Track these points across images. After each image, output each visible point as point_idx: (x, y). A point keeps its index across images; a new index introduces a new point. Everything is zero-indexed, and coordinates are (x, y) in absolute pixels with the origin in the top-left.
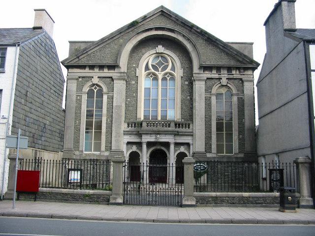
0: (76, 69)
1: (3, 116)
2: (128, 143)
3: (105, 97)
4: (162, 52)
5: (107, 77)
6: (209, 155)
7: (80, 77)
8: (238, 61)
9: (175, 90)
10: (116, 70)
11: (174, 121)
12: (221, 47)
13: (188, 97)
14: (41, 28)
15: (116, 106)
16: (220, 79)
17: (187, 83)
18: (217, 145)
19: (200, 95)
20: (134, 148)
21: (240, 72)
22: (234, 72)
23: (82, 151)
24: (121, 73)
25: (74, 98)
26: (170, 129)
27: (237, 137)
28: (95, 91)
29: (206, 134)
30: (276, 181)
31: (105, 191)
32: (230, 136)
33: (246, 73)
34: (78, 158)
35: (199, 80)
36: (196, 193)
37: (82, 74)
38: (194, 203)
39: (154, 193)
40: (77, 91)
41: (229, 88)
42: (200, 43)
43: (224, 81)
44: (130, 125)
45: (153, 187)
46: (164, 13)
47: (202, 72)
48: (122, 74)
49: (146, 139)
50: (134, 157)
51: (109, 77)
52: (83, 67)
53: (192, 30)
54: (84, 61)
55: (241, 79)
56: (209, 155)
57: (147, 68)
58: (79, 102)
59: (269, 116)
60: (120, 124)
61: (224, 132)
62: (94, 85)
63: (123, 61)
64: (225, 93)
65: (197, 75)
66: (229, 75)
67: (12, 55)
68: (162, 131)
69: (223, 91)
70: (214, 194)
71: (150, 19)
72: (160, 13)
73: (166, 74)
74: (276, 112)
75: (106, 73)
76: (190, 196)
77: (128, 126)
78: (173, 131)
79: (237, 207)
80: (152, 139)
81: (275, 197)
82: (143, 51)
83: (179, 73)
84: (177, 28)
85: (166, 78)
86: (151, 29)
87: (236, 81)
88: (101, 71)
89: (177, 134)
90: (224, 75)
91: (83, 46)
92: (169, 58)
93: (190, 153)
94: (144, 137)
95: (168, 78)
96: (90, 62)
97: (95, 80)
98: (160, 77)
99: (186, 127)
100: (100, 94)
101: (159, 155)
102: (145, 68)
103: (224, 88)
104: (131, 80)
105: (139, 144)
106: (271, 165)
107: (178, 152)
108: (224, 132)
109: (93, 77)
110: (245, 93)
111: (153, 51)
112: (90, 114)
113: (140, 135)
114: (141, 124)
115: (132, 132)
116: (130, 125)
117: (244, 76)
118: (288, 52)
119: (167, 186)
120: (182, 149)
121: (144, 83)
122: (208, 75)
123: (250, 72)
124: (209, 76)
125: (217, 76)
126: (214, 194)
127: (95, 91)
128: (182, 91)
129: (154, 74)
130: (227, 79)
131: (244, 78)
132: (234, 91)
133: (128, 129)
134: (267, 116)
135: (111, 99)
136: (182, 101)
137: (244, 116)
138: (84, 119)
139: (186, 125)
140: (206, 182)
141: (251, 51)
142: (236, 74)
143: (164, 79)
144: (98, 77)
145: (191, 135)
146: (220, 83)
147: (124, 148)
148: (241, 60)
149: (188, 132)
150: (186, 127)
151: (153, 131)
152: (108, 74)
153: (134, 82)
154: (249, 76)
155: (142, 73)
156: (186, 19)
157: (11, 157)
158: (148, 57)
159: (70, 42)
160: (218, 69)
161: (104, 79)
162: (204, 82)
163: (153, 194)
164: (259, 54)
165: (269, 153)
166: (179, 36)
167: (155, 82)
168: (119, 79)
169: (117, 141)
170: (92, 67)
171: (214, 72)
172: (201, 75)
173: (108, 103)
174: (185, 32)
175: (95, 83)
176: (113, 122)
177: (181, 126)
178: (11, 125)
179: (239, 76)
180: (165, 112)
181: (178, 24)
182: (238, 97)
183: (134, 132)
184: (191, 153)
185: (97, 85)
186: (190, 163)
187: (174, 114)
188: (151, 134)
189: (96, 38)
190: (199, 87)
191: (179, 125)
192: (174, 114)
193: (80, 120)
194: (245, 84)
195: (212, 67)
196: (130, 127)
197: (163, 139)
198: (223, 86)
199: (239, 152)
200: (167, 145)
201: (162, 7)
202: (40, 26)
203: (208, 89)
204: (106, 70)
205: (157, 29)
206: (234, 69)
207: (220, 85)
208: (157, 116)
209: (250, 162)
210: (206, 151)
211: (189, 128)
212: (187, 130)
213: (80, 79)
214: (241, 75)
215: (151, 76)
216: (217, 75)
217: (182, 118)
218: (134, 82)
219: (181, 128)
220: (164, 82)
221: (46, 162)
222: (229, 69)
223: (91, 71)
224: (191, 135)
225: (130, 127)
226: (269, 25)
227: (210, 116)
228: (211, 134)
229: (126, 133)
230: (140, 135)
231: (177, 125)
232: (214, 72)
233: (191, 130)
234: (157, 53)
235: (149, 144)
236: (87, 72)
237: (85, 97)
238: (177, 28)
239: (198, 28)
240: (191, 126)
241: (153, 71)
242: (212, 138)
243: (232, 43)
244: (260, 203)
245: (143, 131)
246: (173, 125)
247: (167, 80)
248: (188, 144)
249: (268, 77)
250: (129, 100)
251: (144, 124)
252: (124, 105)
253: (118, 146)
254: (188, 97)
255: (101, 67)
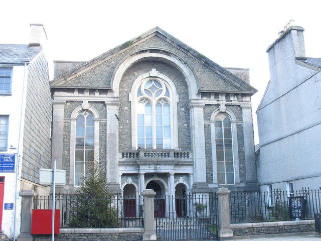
0: (66, 93)
1: (11, 146)
2: (124, 175)
3: (97, 124)
4: (156, 76)
5: (98, 102)
6: (211, 186)
7: (67, 102)
8: (236, 87)
9: (171, 116)
10: (109, 94)
11: (173, 150)
12: (219, 73)
13: (186, 125)
14: (38, 45)
15: (110, 134)
16: (219, 105)
17: (183, 109)
18: (218, 175)
19: (199, 123)
20: (130, 181)
21: (238, 99)
22: (232, 98)
23: (73, 185)
24: (114, 97)
25: (62, 125)
26: (170, 159)
27: (237, 166)
28: (85, 117)
29: (206, 164)
30: (298, 209)
31: (136, 229)
32: (230, 164)
33: (244, 99)
34: (68, 193)
35: (198, 106)
36: (232, 225)
37: (76, 98)
38: (231, 235)
39: (189, 227)
40: (65, 117)
41: (91, 113)
42: (197, 66)
43: (223, 108)
44: (125, 155)
45: (187, 221)
46: (158, 35)
47: (200, 98)
48: (116, 99)
49: (144, 170)
50: (130, 189)
51: (101, 102)
52: (71, 90)
53: (189, 54)
54: (71, 82)
55: (239, 106)
56: (211, 186)
57: (139, 92)
58: (67, 129)
59: (276, 143)
60: (114, 155)
61: (225, 161)
62: (83, 110)
63: (115, 85)
64: (224, 120)
65: (195, 101)
66: (227, 101)
67: (19, 75)
68: (161, 161)
69: (222, 118)
70: (250, 225)
71: (144, 40)
72: (154, 34)
73: (160, 99)
74: (285, 140)
75: (98, 97)
76: (226, 228)
77: (123, 157)
78: (173, 161)
79: (274, 237)
80: (151, 170)
81: (310, 225)
82: (136, 74)
83: (174, 98)
84: (173, 51)
85: (159, 103)
86: (146, 51)
87: (234, 107)
88: (92, 95)
89: (177, 164)
90: (223, 100)
91: (70, 67)
92: (162, 83)
93: (189, 184)
94: (142, 167)
95: (163, 104)
96: (79, 85)
97: (86, 105)
98: (154, 102)
99: (184, 157)
100: (92, 121)
101: (156, 184)
102: (138, 94)
103: (222, 114)
104: (124, 105)
105: (135, 176)
106: (301, 192)
107: (177, 183)
108: (225, 161)
109: (82, 102)
110: (243, 119)
111: (147, 75)
112: (80, 144)
113: (137, 165)
114: (138, 154)
115: (128, 162)
116: (125, 155)
117: (241, 103)
118: (303, 80)
119: (168, 220)
120: (181, 180)
121: (138, 108)
122: (205, 101)
123: (247, 99)
124: (208, 102)
125: (215, 102)
126: (250, 225)
127: (85, 117)
128: (179, 118)
129: (147, 99)
130: (226, 105)
131: (242, 104)
132: (96, 115)
133: (123, 160)
134: (274, 144)
135: (104, 126)
136: (180, 130)
137: (243, 144)
138: (73, 150)
139: (184, 155)
140: (208, 215)
141: (247, 77)
142: (234, 100)
143: (158, 104)
144: (89, 102)
145: (191, 164)
146: (219, 110)
147: (119, 180)
148: (238, 85)
149: (188, 162)
150: (184, 157)
151: (152, 161)
152: (99, 98)
153: (126, 108)
154: (248, 103)
155: (134, 97)
156: (185, 43)
157: (24, 193)
158: (141, 80)
159: (55, 62)
160: (217, 94)
161: (95, 104)
162: (63, 106)
163: (187, 229)
164: (259, 79)
165: (277, 180)
166: (175, 59)
167: (149, 108)
168: (112, 104)
169: (113, 173)
170: (81, 91)
171: (212, 98)
172: (200, 101)
173: (101, 131)
174: (181, 55)
175: (85, 108)
176: (107, 151)
177: (179, 155)
178: (22, 156)
179: (236, 103)
180: (160, 139)
181: (174, 47)
182: (237, 125)
183: (130, 162)
184: (192, 184)
185: (87, 110)
186: (224, 194)
187: (171, 142)
188: (150, 164)
189: (87, 59)
190: (197, 114)
191: (178, 154)
192: (171, 142)
193: (69, 150)
194: (244, 110)
195: (210, 93)
196: (132, 158)
197: (163, 169)
198: (221, 112)
199: (240, 182)
200: (166, 176)
201: (157, 28)
202: (37, 42)
203: (207, 117)
204: (97, 94)
205: (152, 51)
206: (232, 96)
207: (218, 112)
208: (152, 145)
209: (252, 192)
210: (207, 181)
211: (188, 157)
212: (186, 159)
213: (68, 104)
214: (239, 101)
215: (144, 102)
216: (216, 101)
217: (179, 147)
218: (126, 108)
219: (179, 158)
220: (159, 108)
221: (314, 192)
222: (227, 95)
223: (80, 95)
224: (191, 165)
225: (132, 158)
226: (274, 52)
227: (210, 144)
228: (212, 164)
229: (122, 164)
230: (137, 165)
231: (177, 154)
232: (212, 98)
233: (190, 160)
234: (150, 77)
235: (147, 175)
236: (75, 96)
237: (74, 124)
238: (173, 51)
239: (195, 52)
240: (190, 155)
241: (146, 95)
242: (213, 168)
243: (229, 69)
244: (294, 232)
245: (140, 161)
246: (172, 154)
247: (161, 105)
248: (187, 175)
249: (273, 104)
250: (122, 127)
251: (142, 154)
252: (118, 133)
253: (114, 179)
254: (186, 125)
255: (92, 91)
